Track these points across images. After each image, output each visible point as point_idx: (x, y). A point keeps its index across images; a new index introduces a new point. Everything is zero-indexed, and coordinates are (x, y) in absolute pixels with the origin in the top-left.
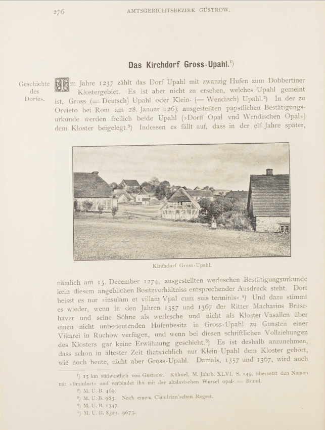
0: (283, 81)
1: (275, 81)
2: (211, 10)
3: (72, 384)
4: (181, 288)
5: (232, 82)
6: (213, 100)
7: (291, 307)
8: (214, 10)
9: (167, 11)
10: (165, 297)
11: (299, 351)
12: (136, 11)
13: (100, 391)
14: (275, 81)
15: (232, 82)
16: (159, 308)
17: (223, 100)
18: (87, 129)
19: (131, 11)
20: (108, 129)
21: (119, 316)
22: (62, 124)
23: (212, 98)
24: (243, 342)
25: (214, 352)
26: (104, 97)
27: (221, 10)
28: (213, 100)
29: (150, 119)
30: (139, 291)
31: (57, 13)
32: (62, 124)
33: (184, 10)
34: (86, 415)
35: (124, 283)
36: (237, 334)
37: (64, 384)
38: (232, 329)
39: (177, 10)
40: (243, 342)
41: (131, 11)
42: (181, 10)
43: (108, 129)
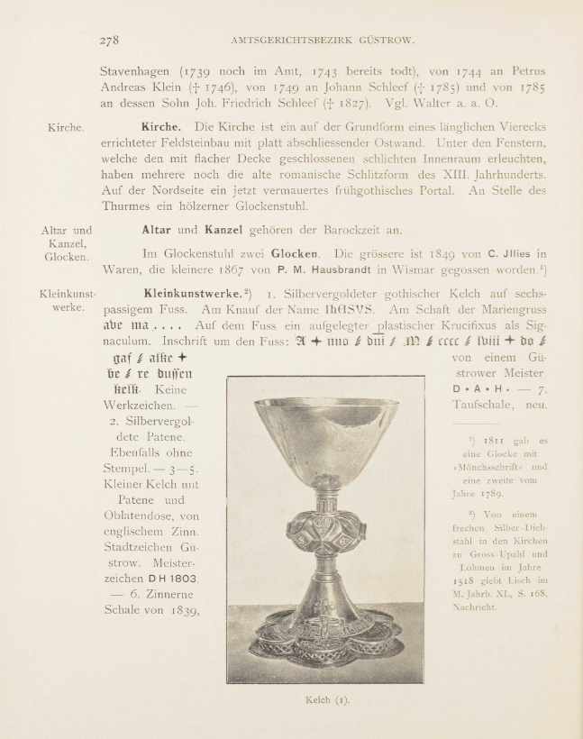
2: (381, 40)
5: (330, 311)
6: (115, 407)
8: (386, 41)
9: (302, 40)
11: (273, 231)
12: (248, 40)
15: (330, 311)
17: (376, 128)
18: (193, 144)
19: (238, 40)
24: (131, 192)
25: (191, 271)
26: (156, 80)
27: (398, 40)
30: (328, 231)
31: (107, 41)
33: (333, 40)
36: (195, 342)
37: (390, 232)
38: (260, 152)
39: (320, 40)
40: (131, 192)
41: (238, 40)
42: (327, 40)
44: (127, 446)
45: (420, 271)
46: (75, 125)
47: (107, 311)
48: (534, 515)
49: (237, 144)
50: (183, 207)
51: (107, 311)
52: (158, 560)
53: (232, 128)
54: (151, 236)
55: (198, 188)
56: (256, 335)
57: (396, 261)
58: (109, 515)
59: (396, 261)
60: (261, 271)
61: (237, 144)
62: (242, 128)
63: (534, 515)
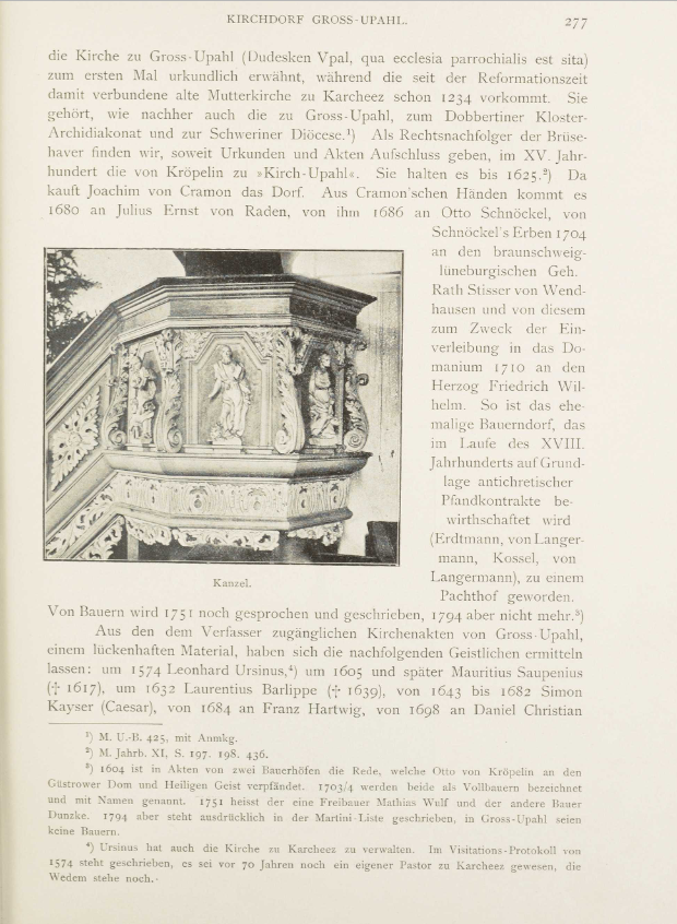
0: (468, 156)
1: (461, 118)
3: (511, 233)
4: (501, 269)
6: (557, 293)
7: (552, 138)
10: (53, 608)
13: (178, 753)
14: (461, 118)
16: (450, 635)
18: (438, 635)
20: (394, 850)
21: (572, 95)
22: (573, 71)
23: (553, 287)
28: (557, 293)
29: (542, 215)
32: (573, 71)
34: (104, 757)
35: (412, 655)
43: (394, 850)
44: (562, 262)
45: (485, 578)
46: (419, 768)
47: (455, 60)
48: (408, 850)
49: (541, 617)
50: (435, 406)
51: (455, 60)
52: (458, 668)
53: (237, 849)
54: (235, 782)
55: (193, 93)
56: (428, 778)
57: (427, 794)
58: (437, 771)
59: (427, 794)
60: (575, 215)
61: (541, 617)
62: (72, 134)
63: (408, 850)
